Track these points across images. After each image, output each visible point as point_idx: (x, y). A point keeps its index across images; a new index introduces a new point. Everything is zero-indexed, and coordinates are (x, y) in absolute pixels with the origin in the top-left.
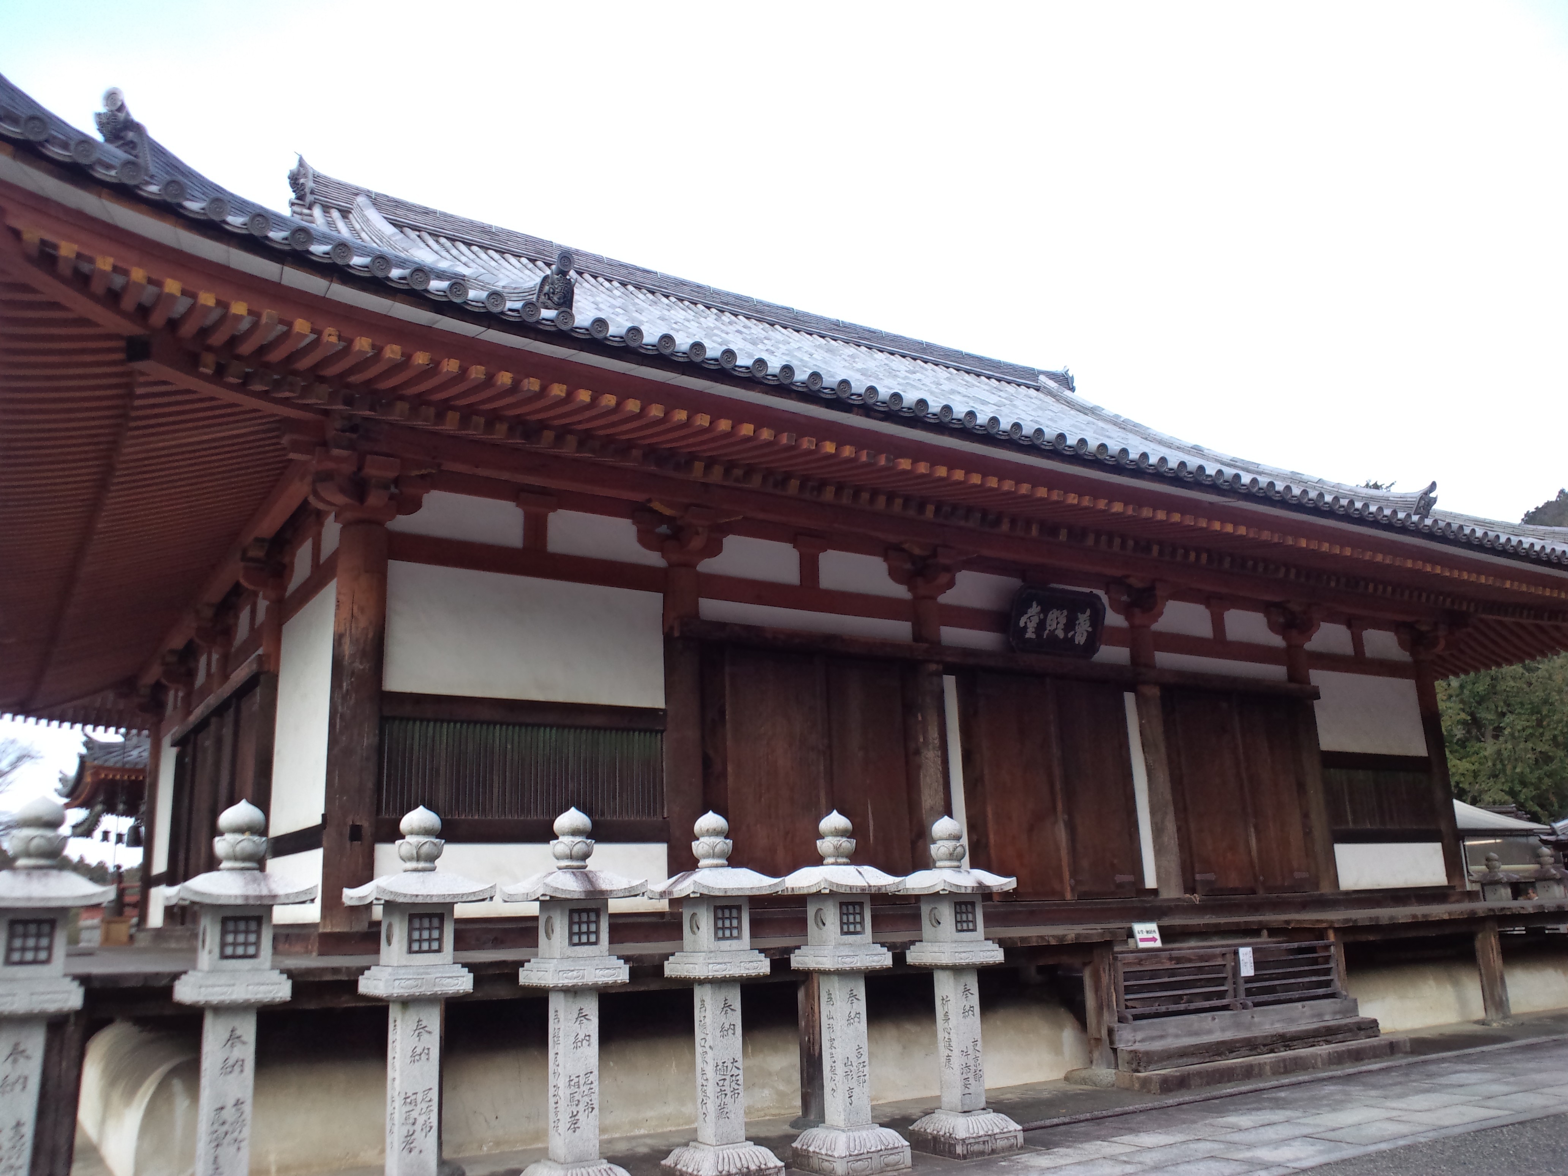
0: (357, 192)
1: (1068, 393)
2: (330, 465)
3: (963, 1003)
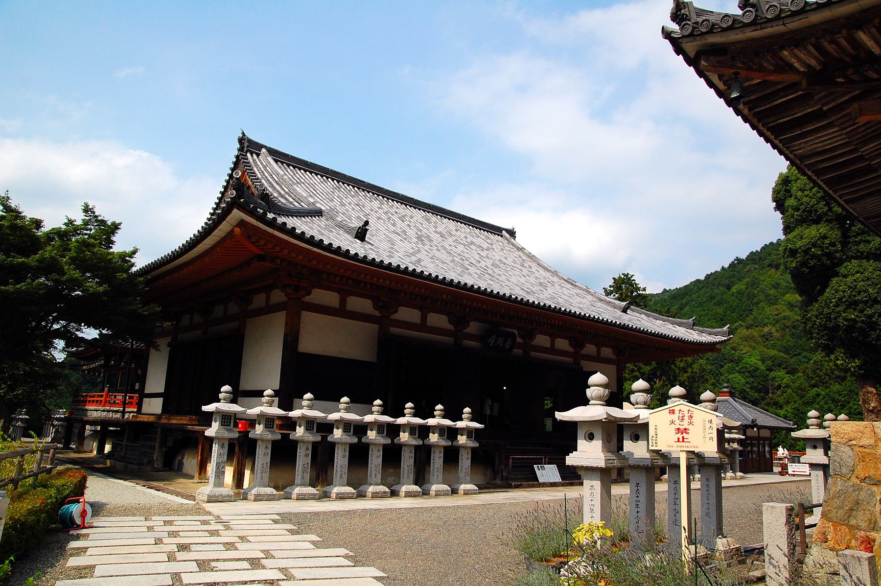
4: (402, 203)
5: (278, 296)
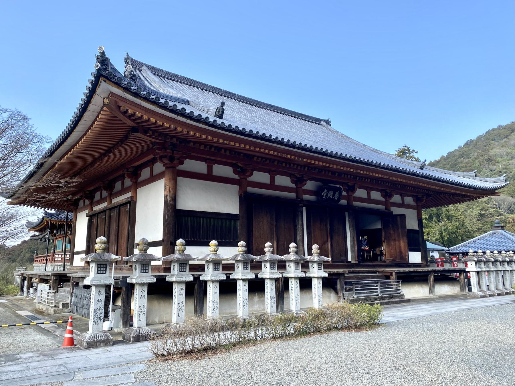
0: (143, 64)
1: (329, 127)
2: (166, 154)
3: (214, 290)
4: (249, 104)
5: (159, 167)
